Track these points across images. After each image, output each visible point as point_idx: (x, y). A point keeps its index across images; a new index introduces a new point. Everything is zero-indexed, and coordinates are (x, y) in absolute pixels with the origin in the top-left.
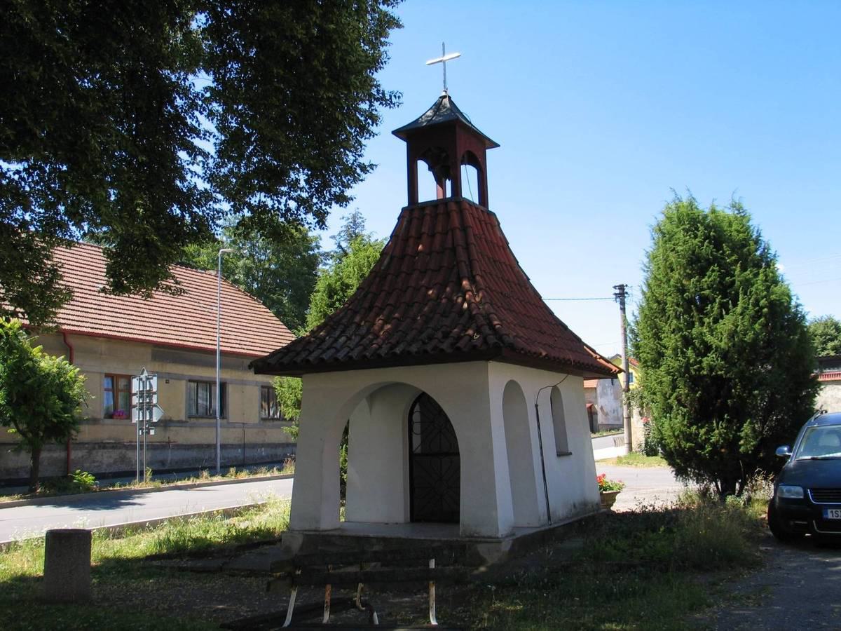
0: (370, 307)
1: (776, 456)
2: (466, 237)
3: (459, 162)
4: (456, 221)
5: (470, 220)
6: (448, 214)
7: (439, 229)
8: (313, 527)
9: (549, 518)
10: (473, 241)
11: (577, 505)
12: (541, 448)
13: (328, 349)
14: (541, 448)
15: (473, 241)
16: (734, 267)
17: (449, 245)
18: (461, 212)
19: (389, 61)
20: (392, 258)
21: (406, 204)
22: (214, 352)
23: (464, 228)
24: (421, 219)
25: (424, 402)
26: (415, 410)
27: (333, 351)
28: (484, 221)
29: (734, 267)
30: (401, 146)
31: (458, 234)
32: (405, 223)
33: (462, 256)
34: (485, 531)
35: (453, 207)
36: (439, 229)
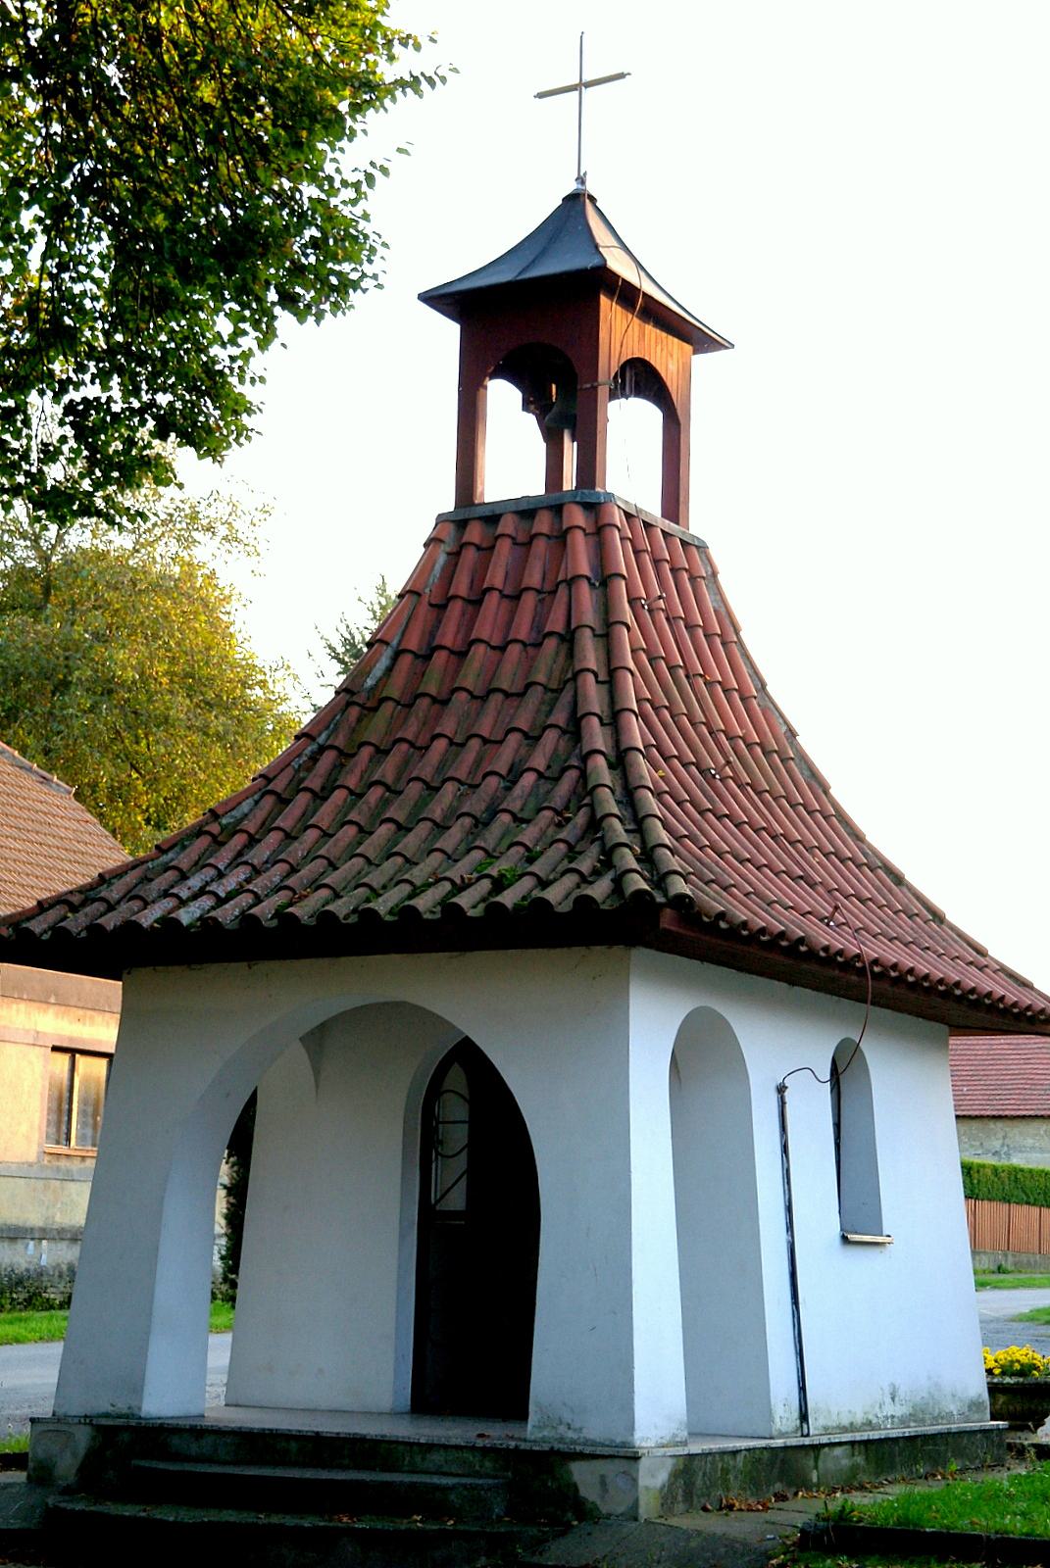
0: (323, 788)
1: (191, 926)
2: (606, 607)
3: (603, 392)
4: (582, 560)
5: (621, 558)
6: (561, 538)
7: (534, 578)
8: (122, 1407)
9: (804, 1417)
10: (629, 617)
11: (901, 1394)
12: (789, 1209)
13: (195, 897)
14: (789, 1209)
15: (629, 617)
16: (156, 925)
17: (556, 623)
18: (599, 531)
19: (373, 291)
20: (397, 655)
21: (449, 505)
22: (873, 1004)
23: (604, 580)
24: (487, 550)
25: (468, 1056)
26: (448, 1084)
27: (206, 902)
28: (671, 562)
29: (156, 925)
30: (447, 333)
31: (586, 596)
32: (442, 559)
33: (590, 655)
34: (595, 1429)
35: (577, 517)
36: (534, 578)
